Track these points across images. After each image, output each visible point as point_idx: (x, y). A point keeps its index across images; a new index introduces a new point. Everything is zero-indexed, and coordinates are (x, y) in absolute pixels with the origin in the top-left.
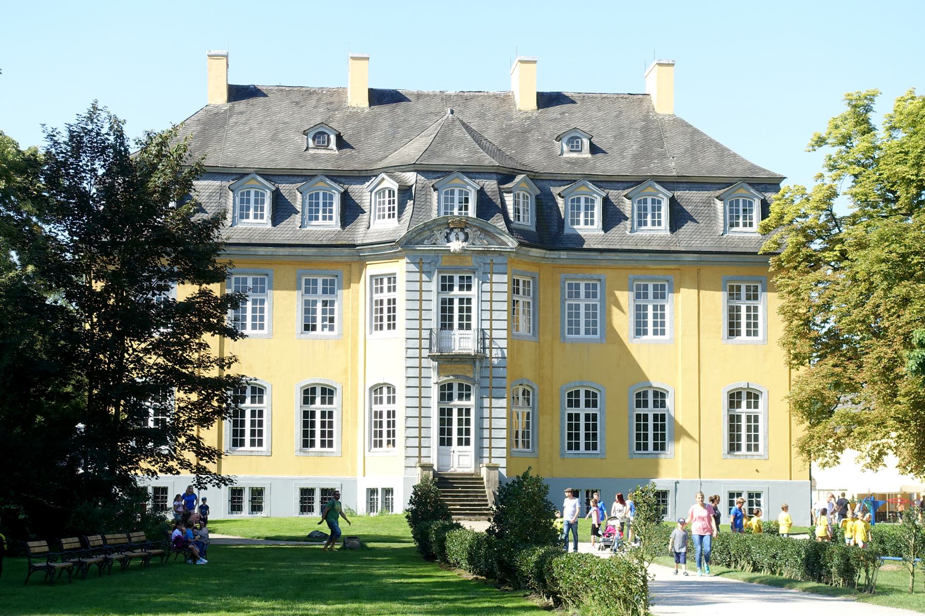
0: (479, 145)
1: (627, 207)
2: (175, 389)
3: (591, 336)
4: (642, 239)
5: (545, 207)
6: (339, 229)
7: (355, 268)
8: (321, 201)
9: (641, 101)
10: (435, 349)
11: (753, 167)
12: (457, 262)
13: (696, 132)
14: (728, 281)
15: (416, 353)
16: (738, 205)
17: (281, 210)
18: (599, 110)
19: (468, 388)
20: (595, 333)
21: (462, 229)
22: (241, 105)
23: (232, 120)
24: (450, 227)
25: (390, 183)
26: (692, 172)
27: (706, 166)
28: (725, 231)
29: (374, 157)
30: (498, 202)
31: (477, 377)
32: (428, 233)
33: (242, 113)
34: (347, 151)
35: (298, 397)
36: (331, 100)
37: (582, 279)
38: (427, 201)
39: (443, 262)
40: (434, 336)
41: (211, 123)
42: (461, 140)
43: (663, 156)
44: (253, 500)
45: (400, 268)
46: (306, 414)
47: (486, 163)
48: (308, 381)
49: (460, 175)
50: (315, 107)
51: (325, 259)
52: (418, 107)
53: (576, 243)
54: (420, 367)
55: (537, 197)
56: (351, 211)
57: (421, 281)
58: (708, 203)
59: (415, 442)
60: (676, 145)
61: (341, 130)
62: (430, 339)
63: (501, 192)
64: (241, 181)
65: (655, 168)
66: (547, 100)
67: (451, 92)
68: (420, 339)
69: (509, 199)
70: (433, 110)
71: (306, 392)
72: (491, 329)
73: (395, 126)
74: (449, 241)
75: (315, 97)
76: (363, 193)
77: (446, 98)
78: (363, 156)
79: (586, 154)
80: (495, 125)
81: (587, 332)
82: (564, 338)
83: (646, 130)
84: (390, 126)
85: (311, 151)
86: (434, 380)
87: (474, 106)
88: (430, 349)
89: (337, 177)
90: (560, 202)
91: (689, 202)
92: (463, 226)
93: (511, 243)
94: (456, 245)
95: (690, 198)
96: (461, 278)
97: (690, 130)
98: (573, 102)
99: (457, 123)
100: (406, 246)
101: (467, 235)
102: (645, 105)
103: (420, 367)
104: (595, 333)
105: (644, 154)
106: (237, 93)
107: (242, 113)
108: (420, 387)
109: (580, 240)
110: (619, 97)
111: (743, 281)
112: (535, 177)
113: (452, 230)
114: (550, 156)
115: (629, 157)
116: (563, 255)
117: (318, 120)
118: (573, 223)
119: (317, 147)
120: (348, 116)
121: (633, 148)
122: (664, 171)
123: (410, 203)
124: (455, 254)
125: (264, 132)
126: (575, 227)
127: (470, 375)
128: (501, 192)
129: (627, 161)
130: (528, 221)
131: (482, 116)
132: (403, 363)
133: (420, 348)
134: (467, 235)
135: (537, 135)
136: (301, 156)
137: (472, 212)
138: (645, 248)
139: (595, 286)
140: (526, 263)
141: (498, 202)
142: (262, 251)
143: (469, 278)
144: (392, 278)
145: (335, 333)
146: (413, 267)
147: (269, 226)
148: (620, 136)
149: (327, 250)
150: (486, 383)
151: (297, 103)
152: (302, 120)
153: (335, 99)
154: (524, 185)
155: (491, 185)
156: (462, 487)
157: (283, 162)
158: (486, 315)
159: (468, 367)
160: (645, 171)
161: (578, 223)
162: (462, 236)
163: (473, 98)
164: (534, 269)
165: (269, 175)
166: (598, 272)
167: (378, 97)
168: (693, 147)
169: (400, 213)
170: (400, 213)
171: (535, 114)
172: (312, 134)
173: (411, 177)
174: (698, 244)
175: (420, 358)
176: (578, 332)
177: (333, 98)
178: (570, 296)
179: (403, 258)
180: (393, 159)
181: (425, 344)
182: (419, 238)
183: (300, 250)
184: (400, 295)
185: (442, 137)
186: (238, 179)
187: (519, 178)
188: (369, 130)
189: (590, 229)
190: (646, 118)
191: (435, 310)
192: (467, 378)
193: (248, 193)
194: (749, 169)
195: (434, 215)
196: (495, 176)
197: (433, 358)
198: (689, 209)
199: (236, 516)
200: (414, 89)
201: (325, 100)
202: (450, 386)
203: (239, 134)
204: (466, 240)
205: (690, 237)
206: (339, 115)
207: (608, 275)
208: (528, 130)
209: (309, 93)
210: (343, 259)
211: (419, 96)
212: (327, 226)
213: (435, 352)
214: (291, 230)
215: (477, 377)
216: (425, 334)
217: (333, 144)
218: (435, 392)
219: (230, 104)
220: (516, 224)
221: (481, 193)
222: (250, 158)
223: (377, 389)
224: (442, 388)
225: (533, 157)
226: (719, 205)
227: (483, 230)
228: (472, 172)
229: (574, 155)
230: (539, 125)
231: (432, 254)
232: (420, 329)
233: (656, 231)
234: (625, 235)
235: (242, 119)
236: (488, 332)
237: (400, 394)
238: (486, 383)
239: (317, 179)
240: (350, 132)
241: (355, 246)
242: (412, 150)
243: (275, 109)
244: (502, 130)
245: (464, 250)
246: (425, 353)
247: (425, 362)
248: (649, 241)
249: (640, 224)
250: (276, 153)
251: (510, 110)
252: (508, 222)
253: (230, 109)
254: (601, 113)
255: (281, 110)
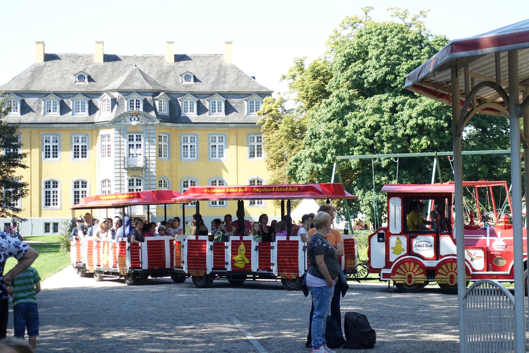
0: (146, 80)
1: (207, 105)
2: (359, 193)
3: (193, 158)
4: (213, 118)
5: (174, 106)
6: (88, 116)
7: (95, 132)
8: (80, 104)
9: (219, 58)
10: (126, 165)
11: (262, 87)
12: (135, 129)
13: (240, 71)
14: (249, 135)
15: (119, 167)
16: (253, 103)
17: (64, 109)
18: (201, 62)
19: (140, 181)
20: (194, 157)
21: (137, 116)
22: (49, 63)
23: (45, 70)
24: (132, 115)
25: (108, 97)
26: (235, 89)
27: (242, 87)
28: (248, 114)
29: (103, 85)
30: (152, 104)
31: (144, 176)
32: (123, 118)
33: (49, 66)
34: (92, 83)
35: (73, 185)
36: (87, 60)
37: (189, 135)
38: (123, 104)
39: (129, 129)
40: (126, 160)
41: (36, 72)
42: (138, 78)
43: (224, 82)
44: (54, 228)
45: (112, 132)
46: (75, 192)
47: (147, 88)
48: (76, 179)
49: (136, 93)
50: (81, 63)
51: (82, 128)
52: (124, 62)
53: (187, 121)
54: (120, 172)
55: (170, 102)
56: (93, 109)
57: (120, 137)
58: (241, 103)
59: (119, 143)
60: (231, 77)
61: (90, 74)
62: (124, 161)
63: (154, 100)
64: (46, 97)
65: (220, 89)
66: (179, 58)
67: (139, 55)
68: (120, 161)
69: (157, 103)
70: (130, 63)
71: (75, 183)
72: (149, 157)
73: (113, 71)
74: (131, 121)
75: (81, 59)
76: (97, 102)
77: (137, 58)
78: (98, 85)
79: (192, 82)
80: (156, 69)
81: (191, 156)
82: (181, 159)
83: (219, 71)
84: (112, 71)
85: (77, 83)
86: (126, 178)
87: (148, 61)
88: (124, 165)
89: (85, 94)
90: (180, 102)
91: (233, 102)
92: (137, 114)
93: (157, 122)
94: (134, 123)
95: (234, 102)
96: (137, 136)
97: (238, 70)
98: (190, 59)
99: (138, 70)
100: (115, 123)
101: (138, 118)
102: (221, 59)
103: (120, 172)
104: (194, 157)
105: (217, 82)
106: (49, 57)
107: (49, 66)
108: (120, 181)
109: (187, 118)
110: (210, 56)
111: (255, 135)
112: (168, 93)
113: (132, 116)
114: (177, 83)
115: (210, 83)
116: (180, 125)
117: (81, 69)
118: (185, 112)
119: (80, 81)
120: (94, 67)
121: (212, 79)
122: (224, 89)
123: (116, 105)
124: (134, 126)
125: (58, 75)
126: (186, 113)
127: (141, 175)
128: (154, 100)
129: (209, 85)
130: (165, 111)
131: (151, 65)
132: (113, 167)
133: (120, 165)
134: (138, 118)
135: (172, 74)
136: (73, 85)
137: (141, 109)
138: (214, 122)
139: (194, 138)
140: (164, 129)
141: (152, 104)
142: (56, 126)
143: (140, 136)
144: (109, 136)
145: (182, 145)
146: (117, 132)
147: (59, 115)
148: (208, 74)
149: (83, 125)
150: (147, 178)
151: (73, 61)
152: (74, 69)
153: (89, 59)
154: (163, 97)
155: (149, 98)
156: (285, 251)
157: (65, 88)
158: (147, 151)
159: (140, 172)
160: (216, 89)
161: (187, 112)
162: (137, 119)
163: (148, 58)
164: (168, 131)
165: (57, 94)
166: (195, 132)
167: (108, 58)
168: (238, 78)
169: (112, 110)
170: (112, 110)
171: (174, 64)
172: (77, 76)
173: (116, 95)
174: (236, 120)
175: (120, 168)
176: (187, 157)
177: (87, 59)
178: (184, 142)
179: (113, 128)
180: (110, 87)
181: (122, 163)
182: (119, 120)
183: (71, 125)
184: (112, 143)
185: (131, 77)
186: (45, 96)
187: (161, 94)
188: (102, 73)
189: (192, 115)
190: (220, 66)
191: (126, 149)
192: (139, 177)
193: (50, 102)
194: (259, 88)
195: (126, 110)
196: (151, 94)
197: (125, 168)
198: (233, 105)
199: (47, 234)
200: (124, 54)
201: (85, 60)
202: (133, 180)
203: (48, 76)
204: (138, 120)
205: (233, 117)
206: (90, 66)
207: (199, 133)
208: (170, 72)
209: (79, 57)
210: (90, 128)
211: (125, 57)
212: (83, 115)
213: (126, 167)
214: (68, 117)
215: (144, 176)
216: (122, 159)
217: (86, 80)
218: (126, 183)
219: (45, 62)
220: (160, 113)
221: (145, 101)
222: (51, 87)
223: (104, 181)
224: (130, 181)
225: (171, 85)
226: (246, 103)
227: (145, 116)
228: (140, 92)
229: (188, 83)
230: (174, 69)
231: (125, 126)
232: (120, 157)
233: (220, 116)
234: (205, 117)
235: (49, 69)
236: (148, 158)
237: (113, 183)
238: (147, 178)
239: (78, 96)
240: (94, 74)
241: (94, 123)
242: (117, 83)
243: (63, 64)
244: (159, 72)
245: (137, 124)
246: (122, 167)
247: (122, 170)
248: (216, 119)
249: (213, 112)
250: (63, 84)
251: (163, 63)
252: (156, 113)
253: (45, 65)
254: (201, 63)
255: (65, 64)
